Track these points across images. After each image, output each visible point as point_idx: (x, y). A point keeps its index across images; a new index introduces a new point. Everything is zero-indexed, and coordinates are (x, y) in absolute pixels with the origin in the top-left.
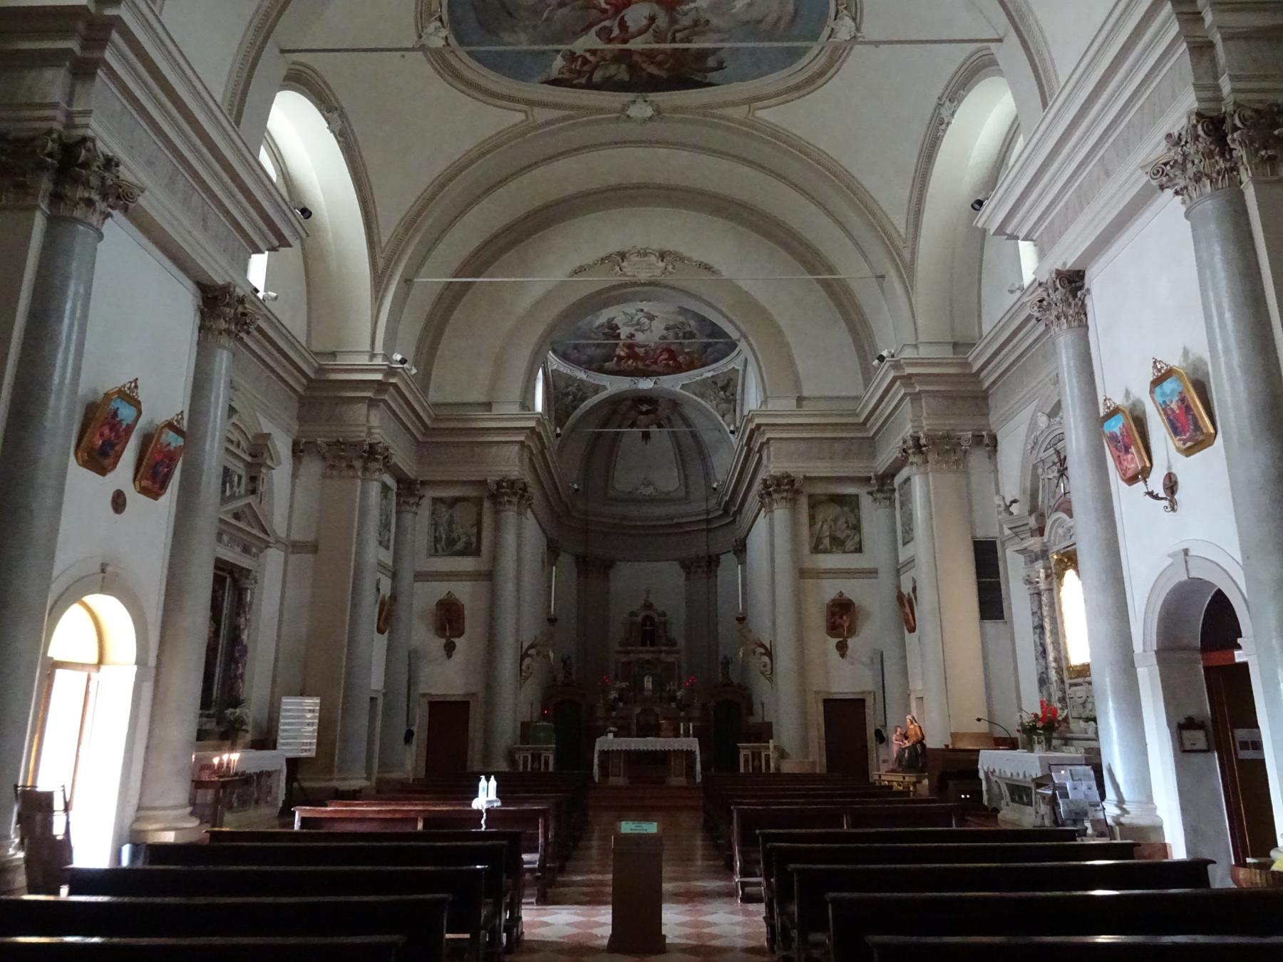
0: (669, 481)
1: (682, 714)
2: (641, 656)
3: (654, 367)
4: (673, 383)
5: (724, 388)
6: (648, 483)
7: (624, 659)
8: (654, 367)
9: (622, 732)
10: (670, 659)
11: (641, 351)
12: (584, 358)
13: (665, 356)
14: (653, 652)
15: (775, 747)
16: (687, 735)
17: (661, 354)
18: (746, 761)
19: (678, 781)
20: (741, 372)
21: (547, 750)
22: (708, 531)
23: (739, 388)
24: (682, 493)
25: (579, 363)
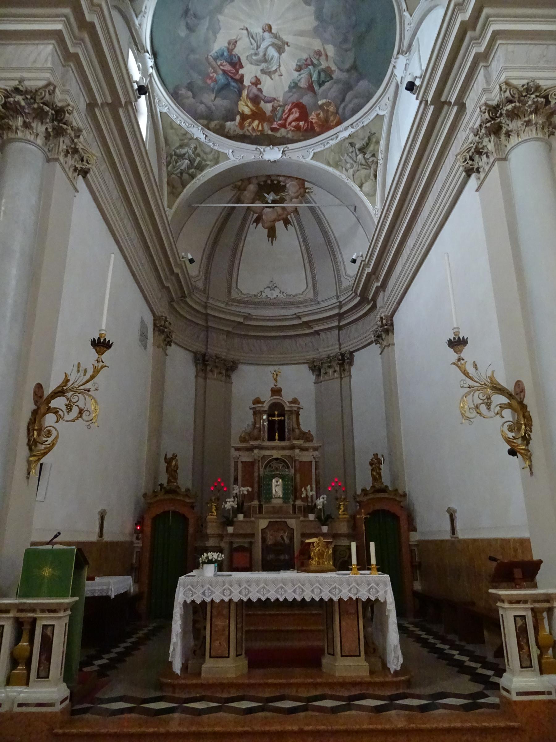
0: (294, 283)
1: (325, 529)
2: (267, 453)
4: (303, 154)
5: (362, 150)
6: (273, 287)
7: (246, 457)
9: (237, 559)
10: (306, 457)
11: (267, 108)
12: (201, 108)
13: (296, 114)
14: (284, 448)
16: (364, 564)
18: (522, 632)
19: (348, 667)
20: (386, 119)
21: (52, 610)
22: (340, 328)
23: (382, 143)
24: (311, 295)
25: (196, 116)
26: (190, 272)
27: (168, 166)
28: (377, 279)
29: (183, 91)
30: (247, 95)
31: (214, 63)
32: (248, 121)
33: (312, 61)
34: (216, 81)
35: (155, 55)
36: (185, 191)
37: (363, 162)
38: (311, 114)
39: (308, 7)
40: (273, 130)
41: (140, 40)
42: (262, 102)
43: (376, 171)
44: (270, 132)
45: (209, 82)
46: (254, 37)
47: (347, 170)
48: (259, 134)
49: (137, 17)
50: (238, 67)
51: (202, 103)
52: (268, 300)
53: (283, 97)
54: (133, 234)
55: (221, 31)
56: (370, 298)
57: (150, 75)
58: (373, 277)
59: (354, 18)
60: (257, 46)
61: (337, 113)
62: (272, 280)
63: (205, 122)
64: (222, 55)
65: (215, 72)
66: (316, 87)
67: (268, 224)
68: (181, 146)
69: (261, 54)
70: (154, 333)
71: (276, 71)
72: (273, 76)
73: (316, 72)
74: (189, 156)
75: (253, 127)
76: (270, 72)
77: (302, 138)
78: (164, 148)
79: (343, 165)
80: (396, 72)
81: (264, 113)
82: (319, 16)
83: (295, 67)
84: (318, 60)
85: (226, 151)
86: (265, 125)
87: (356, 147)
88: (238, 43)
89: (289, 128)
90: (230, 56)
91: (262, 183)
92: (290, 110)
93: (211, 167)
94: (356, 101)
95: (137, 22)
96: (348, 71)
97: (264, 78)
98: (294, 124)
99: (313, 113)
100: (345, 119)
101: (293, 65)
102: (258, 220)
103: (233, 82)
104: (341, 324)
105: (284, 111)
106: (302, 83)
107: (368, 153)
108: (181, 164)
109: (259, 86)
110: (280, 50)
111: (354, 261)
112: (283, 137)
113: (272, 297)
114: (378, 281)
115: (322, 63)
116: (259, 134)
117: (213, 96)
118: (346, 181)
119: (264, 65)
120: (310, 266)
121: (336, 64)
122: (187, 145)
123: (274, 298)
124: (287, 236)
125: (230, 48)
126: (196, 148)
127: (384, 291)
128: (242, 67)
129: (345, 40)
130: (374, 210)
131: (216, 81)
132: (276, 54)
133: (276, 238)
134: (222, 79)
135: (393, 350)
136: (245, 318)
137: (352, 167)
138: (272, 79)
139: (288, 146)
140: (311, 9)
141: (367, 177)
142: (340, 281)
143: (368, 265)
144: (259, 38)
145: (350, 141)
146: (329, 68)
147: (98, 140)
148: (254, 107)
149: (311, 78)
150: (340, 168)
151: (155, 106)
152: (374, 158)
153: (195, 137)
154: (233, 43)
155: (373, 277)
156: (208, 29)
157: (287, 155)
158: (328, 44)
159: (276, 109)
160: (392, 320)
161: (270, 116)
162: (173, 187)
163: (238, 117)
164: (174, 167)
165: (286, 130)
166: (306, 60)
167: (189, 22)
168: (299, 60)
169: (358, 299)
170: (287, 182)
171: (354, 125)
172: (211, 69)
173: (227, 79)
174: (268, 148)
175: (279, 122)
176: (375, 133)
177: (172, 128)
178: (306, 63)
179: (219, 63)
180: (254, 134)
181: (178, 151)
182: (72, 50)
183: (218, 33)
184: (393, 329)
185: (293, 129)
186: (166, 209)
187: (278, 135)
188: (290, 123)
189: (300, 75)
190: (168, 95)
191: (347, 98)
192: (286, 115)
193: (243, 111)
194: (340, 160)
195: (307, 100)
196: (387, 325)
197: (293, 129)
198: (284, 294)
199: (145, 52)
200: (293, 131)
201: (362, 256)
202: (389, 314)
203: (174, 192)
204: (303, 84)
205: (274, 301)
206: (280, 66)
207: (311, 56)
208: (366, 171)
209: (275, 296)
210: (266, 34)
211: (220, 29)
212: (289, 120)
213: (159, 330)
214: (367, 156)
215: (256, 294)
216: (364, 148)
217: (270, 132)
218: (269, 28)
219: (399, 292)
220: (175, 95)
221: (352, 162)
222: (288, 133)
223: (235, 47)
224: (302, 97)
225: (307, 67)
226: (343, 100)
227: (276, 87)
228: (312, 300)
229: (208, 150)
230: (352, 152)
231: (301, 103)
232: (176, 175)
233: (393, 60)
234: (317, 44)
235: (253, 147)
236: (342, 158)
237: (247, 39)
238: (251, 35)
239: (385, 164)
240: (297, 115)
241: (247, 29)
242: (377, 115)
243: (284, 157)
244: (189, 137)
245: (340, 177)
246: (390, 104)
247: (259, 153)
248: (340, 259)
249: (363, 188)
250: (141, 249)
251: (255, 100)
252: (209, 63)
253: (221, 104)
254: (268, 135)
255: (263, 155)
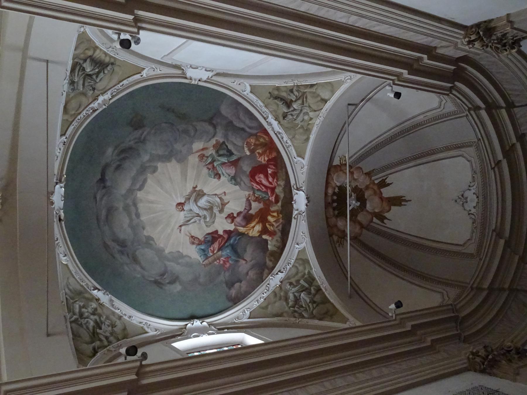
0: (458, 173)
3: (279, 190)
4: (300, 168)
6: (463, 199)
8: (279, 190)
11: (256, 206)
12: (252, 274)
13: (261, 177)
15: (514, 358)
17: (260, 183)
22: (510, 106)
23: (277, 83)
25: (260, 280)
26: (436, 304)
27: (303, 317)
28: (420, 59)
29: (233, 292)
30: (244, 227)
31: (210, 259)
32: (268, 226)
33: (210, 163)
34: (228, 258)
35: (192, 318)
36: (332, 301)
37: (300, 102)
38: (259, 161)
39: (159, 170)
40: (277, 201)
41: (172, 331)
42: (251, 212)
43: (306, 86)
44: (280, 204)
45: (228, 265)
46: (188, 219)
47: (311, 119)
48: (281, 216)
49: (147, 332)
50: (216, 236)
51: (247, 273)
52: (480, 205)
53: (244, 190)
54: (384, 369)
55: (181, 251)
56: (453, 68)
57: (209, 325)
58: (415, 66)
59: (164, 125)
60: (197, 216)
61: (256, 135)
62: (454, 201)
63: (266, 271)
64: (203, 250)
65: (219, 259)
66: (234, 158)
67: (385, 204)
68: (286, 299)
69: (205, 213)
70: (495, 375)
71: (220, 198)
72: (226, 201)
73: (219, 158)
74: (297, 291)
75: (274, 221)
76: (222, 204)
77: (284, 170)
78: (284, 319)
79: (306, 124)
80: (205, 78)
81: (261, 210)
82: (166, 158)
83: (216, 180)
84: (207, 157)
85: (297, 251)
86: (272, 209)
87: (286, 111)
88: (193, 235)
89: (274, 184)
90: (205, 243)
91: (336, 212)
92: (257, 183)
93: (312, 269)
94: (241, 115)
95: (152, 333)
96: (215, 127)
97: (228, 210)
98: (270, 179)
99: (259, 159)
100: (261, 126)
101: (214, 181)
102: (382, 218)
103: (230, 241)
104: (504, 105)
105: (259, 190)
106: (231, 172)
107: (289, 97)
108: (304, 302)
109: (235, 215)
110: (200, 194)
111: (398, 95)
112: (284, 189)
113: (476, 200)
114: (421, 59)
115: (210, 153)
116: (281, 216)
117: (242, 262)
118: (322, 119)
119: (216, 210)
120: (434, 154)
121: (210, 140)
122: (286, 293)
123: (477, 197)
124: (400, 183)
125: (197, 242)
126: (291, 284)
127: (435, 48)
128: (217, 231)
129: (186, 132)
130: (347, 82)
131: (228, 258)
132: (205, 198)
133: (402, 197)
134: (227, 252)
135: (519, 14)
136: (500, 235)
137: (307, 113)
138: (229, 202)
139: (292, 184)
140: (160, 165)
141: (315, 95)
142: (449, 114)
143: (399, 76)
144: (190, 215)
145: (281, 118)
146: (214, 146)
147: (294, 387)
148: (254, 220)
149: (226, 163)
150: (310, 127)
151: (242, 323)
152: (294, 90)
153: (279, 283)
154: (193, 239)
155: (415, 66)
156: (178, 264)
157: (301, 185)
158: (192, 149)
159: (257, 198)
160: (472, 27)
161: (265, 204)
162: (326, 313)
163: (264, 237)
164: (306, 310)
165: (277, 187)
166: (209, 169)
167: (167, 281)
168: (210, 176)
169: (458, 84)
170: (334, 185)
171: (265, 116)
172: (215, 262)
173: (227, 246)
174: (294, 206)
175: (269, 194)
176: (270, 93)
177: (266, 307)
178: (212, 169)
179: (211, 254)
180: (281, 221)
181: (291, 304)
182: (429, 344)
183: (182, 254)
184: (485, 22)
185: (275, 180)
186: (346, 326)
187: (282, 196)
188: (270, 183)
189: (223, 175)
190: (234, 308)
191: (242, 126)
192: (263, 188)
193: (258, 232)
194: (302, 127)
195: (247, 168)
196: (479, 33)
197: (275, 180)
198: (471, 185)
199: (185, 328)
200: (277, 180)
201: (389, 85)
202: (462, 32)
203: (330, 313)
204: (232, 171)
205: (481, 198)
206: (216, 195)
207: (204, 164)
208: (309, 97)
209: (475, 196)
210: (186, 208)
211: (179, 252)
212: (267, 184)
213: (492, 367)
214: (293, 98)
215: (471, 221)
216: (286, 103)
217: (280, 204)
218: (180, 205)
219: (433, 25)
220: (236, 301)
221: (302, 114)
222: (279, 185)
223: (197, 238)
224: (244, 172)
225: (216, 167)
226: (243, 129)
227: (237, 198)
228: (478, 148)
229: (294, 271)
230: (292, 115)
231: (250, 172)
232: (314, 308)
233: (193, 82)
234: (193, 159)
235: (294, 221)
236: (299, 126)
237: (191, 226)
238: (186, 223)
239: (297, 76)
240: (262, 176)
241: (181, 226)
242: (251, 92)
243: (303, 188)
244: (278, 289)
245: (319, 125)
246: (238, 81)
247: (299, 216)
248: (422, 117)
249: (326, 98)
250: (358, 375)
251: (248, 219)
252: (210, 264)
253: (250, 254)
254: (282, 206)
255: (301, 211)
